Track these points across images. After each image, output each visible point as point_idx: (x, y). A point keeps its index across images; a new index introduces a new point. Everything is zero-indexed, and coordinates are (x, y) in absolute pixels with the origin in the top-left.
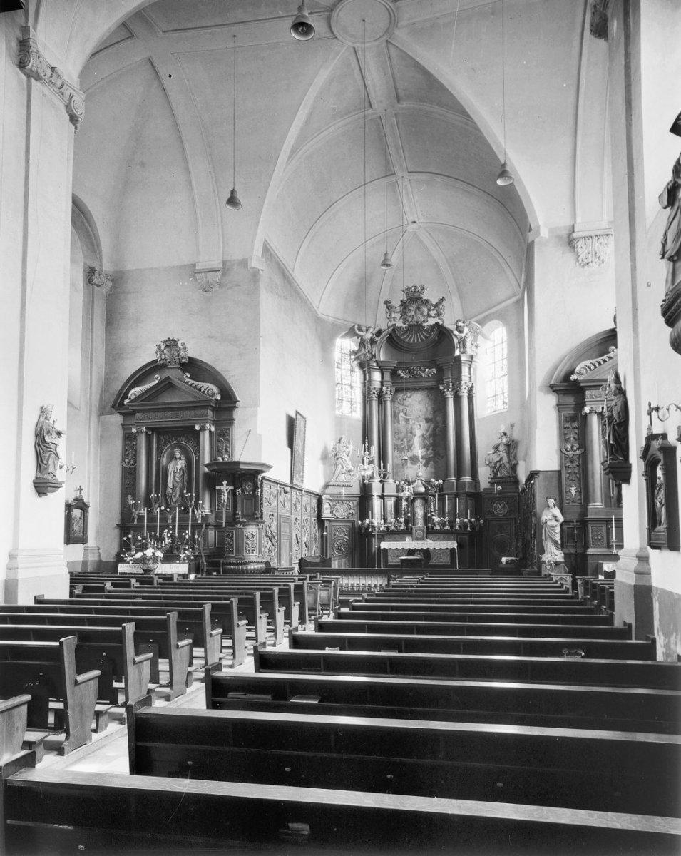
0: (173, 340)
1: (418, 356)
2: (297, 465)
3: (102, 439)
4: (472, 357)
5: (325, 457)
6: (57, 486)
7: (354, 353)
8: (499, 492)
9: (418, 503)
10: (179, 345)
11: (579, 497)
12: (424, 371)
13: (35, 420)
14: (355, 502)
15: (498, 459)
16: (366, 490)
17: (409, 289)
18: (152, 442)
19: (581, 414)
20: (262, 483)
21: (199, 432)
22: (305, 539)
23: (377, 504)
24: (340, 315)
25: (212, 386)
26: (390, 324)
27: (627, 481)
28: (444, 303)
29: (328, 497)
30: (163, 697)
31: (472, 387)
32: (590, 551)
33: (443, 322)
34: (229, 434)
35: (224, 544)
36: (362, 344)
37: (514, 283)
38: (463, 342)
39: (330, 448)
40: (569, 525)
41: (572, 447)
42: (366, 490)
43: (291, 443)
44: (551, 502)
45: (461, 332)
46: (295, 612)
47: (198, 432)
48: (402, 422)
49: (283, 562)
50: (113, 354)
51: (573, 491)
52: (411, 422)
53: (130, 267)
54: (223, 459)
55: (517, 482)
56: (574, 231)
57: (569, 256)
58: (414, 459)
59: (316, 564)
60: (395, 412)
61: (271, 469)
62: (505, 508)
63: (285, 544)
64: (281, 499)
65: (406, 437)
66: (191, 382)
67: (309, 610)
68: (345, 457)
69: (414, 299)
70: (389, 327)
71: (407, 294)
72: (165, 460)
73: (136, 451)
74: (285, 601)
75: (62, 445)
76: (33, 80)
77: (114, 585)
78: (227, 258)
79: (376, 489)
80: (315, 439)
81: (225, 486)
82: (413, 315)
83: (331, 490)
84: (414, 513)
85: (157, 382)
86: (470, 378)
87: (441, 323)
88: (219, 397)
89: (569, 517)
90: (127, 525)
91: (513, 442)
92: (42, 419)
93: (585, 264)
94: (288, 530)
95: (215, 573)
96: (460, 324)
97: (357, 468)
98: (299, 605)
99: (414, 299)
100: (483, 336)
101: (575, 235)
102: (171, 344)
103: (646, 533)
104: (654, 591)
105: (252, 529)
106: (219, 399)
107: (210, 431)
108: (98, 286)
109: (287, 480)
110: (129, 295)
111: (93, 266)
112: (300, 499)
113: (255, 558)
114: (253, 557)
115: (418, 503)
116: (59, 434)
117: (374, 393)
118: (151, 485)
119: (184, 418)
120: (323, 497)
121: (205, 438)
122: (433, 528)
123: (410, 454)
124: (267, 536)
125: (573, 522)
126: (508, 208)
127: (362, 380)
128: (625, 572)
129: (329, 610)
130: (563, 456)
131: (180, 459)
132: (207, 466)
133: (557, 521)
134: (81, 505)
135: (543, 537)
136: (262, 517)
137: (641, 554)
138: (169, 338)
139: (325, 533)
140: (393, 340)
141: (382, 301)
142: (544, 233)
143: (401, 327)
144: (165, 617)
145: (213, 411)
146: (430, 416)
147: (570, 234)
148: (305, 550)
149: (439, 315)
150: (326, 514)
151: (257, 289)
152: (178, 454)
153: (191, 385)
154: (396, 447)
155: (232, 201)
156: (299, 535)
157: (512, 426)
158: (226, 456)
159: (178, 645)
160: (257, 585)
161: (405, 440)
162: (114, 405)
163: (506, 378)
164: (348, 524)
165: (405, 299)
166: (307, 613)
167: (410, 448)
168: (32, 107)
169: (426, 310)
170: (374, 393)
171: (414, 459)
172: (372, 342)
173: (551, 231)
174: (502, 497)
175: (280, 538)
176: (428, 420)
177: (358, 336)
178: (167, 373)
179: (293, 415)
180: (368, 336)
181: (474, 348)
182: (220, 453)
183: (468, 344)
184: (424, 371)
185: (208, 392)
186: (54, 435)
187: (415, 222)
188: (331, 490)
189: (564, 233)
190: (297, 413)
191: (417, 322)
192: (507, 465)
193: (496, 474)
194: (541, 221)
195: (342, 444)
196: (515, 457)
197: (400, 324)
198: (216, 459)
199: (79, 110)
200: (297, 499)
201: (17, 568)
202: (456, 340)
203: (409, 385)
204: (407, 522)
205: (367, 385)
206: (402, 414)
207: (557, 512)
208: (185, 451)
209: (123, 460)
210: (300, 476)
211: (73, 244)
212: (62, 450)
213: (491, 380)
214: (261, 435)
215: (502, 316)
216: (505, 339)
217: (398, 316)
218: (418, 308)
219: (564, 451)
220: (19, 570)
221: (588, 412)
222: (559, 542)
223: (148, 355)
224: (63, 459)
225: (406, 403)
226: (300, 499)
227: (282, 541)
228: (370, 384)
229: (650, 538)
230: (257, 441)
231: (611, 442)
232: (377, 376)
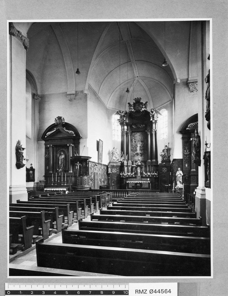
0: (60, 117)
1: (138, 121)
2: (100, 156)
3: (39, 148)
4: (156, 121)
5: (109, 154)
6: (23, 165)
7: (118, 120)
8: (164, 165)
9: (139, 168)
10: (62, 118)
11: (188, 168)
12: (141, 126)
13: (16, 145)
14: (119, 168)
15: (164, 154)
16: (122, 164)
17: (136, 99)
20: (88, 163)
21: (68, 146)
22: (103, 180)
23: (126, 168)
24: (114, 107)
25: (72, 132)
26: (130, 110)
27: (200, 166)
28: (147, 103)
29: (110, 166)
30: (55, 232)
31: (156, 131)
32: (191, 185)
33: (147, 109)
36: (121, 117)
37: (170, 97)
38: (153, 116)
39: (111, 150)
40: (185, 176)
41: (187, 151)
42: (122, 164)
43: (98, 149)
44: (179, 169)
45: (153, 113)
46: (97, 204)
48: (134, 142)
49: (95, 187)
50: (41, 121)
51: (187, 166)
52: (137, 142)
53: (46, 93)
54: (76, 155)
55: (170, 161)
56: (188, 80)
57: (186, 89)
58: (137, 154)
59: (105, 188)
60: (131, 139)
61: (91, 158)
62: (166, 170)
63: (96, 181)
64: (95, 167)
65: (135, 147)
66: (66, 130)
67: (102, 203)
68: (115, 153)
69: (138, 102)
70: (129, 111)
71: (135, 101)
72: (58, 155)
73: (49, 152)
74: (94, 201)
75: (24, 153)
76: (12, 36)
77: (42, 196)
78: (77, 90)
79: (125, 163)
80: (106, 148)
83: (111, 164)
84: (137, 171)
85: (55, 130)
86: (155, 128)
87: (146, 110)
88: (75, 135)
89: (185, 174)
90: (47, 175)
91: (169, 148)
92: (18, 145)
93: (192, 91)
94: (97, 177)
95: (74, 191)
96: (152, 110)
97: (118, 158)
98: (99, 202)
99: (138, 102)
100: (160, 114)
101: (188, 82)
102: (60, 118)
103: (204, 182)
104: (206, 200)
105: (85, 177)
107: (72, 146)
108: (36, 99)
109: (97, 161)
110: (46, 102)
111: (34, 93)
112: (101, 167)
113: (87, 187)
114: (87, 186)
115: (139, 168)
116: (23, 149)
117: (125, 133)
119: (64, 142)
120: (109, 166)
121: (71, 149)
122: (143, 176)
123: (136, 152)
124: (90, 179)
125: (186, 175)
126: (168, 74)
127: (121, 129)
128: (198, 194)
129: (108, 203)
130: (184, 154)
131: (63, 155)
132: (71, 157)
133: (181, 175)
134: (32, 169)
135: (177, 180)
136: (88, 174)
137: (203, 189)
138: (59, 116)
139: (109, 178)
140: (130, 115)
141: (127, 103)
142: (179, 81)
143: (133, 111)
144: (55, 208)
145: (73, 140)
146: (142, 140)
147: (187, 81)
148: (103, 183)
149: (146, 107)
150: (110, 171)
151: (86, 100)
152: (62, 153)
153: (66, 131)
154: (132, 150)
155: (78, 72)
156: (101, 178)
157: (169, 143)
158: (77, 154)
159: (59, 217)
160: (86, 196)
161: (134, 148)
162: (42, 138)
163: (167, 128)
164: (116, 175)
165: (135, 102)
166: (101, 204)
167: (136, 150)
168: (12, 44)
169: (141, 106)
170: (125, 133)
171: (137, 154)
172: (124, 116)
173: (181, 80)
174: (165, 166)
175: (96, 178)
176: (142, 142)
177: (120, 114)
178: (58, 128)
179: (99, 141)
180: (123, 114)
181: (157, 118)
182: (75, 153)
183: (155, 117)
184: (141, 126)
186: (22, 150)
187: (138, 77)
188: (111, 164)
189: (185, 81)
190: (100, 140)
191: (138, 110)
192: (167, 156)
193: (163, 159)
194: (178, 77)
195: (114, 149)
196: (169, 154)
197: (133, 110)
198: (74, 155)
199: (28, 44)
200: (100, 167)
201: (11, 191)
202: (151, 116)
203: (136, 130)
204: (135, 174)
205: (123, 130)
206: (133, 140)
207: (181, 172)
209: (45, 155)
210: (101, 160)
211: (27, 86)
212: (24, 155)
213: (162, 128)
214: (88, 148)
215: (166, 107)
216: (167, 115)
217: (132, 108)
218: (139, 105)
219: (184, 153)
220: (12, 192)
221: (192, 140)
222: (182, 182)
223: (52, 122)
224: (25, 157)
225: (135, 136)
226: (101, 167)
227: (95, 181)
228: (123, 130)
229: (205, 184)
230: (87, 149)
231: (195, 153)
232: (126, 127)
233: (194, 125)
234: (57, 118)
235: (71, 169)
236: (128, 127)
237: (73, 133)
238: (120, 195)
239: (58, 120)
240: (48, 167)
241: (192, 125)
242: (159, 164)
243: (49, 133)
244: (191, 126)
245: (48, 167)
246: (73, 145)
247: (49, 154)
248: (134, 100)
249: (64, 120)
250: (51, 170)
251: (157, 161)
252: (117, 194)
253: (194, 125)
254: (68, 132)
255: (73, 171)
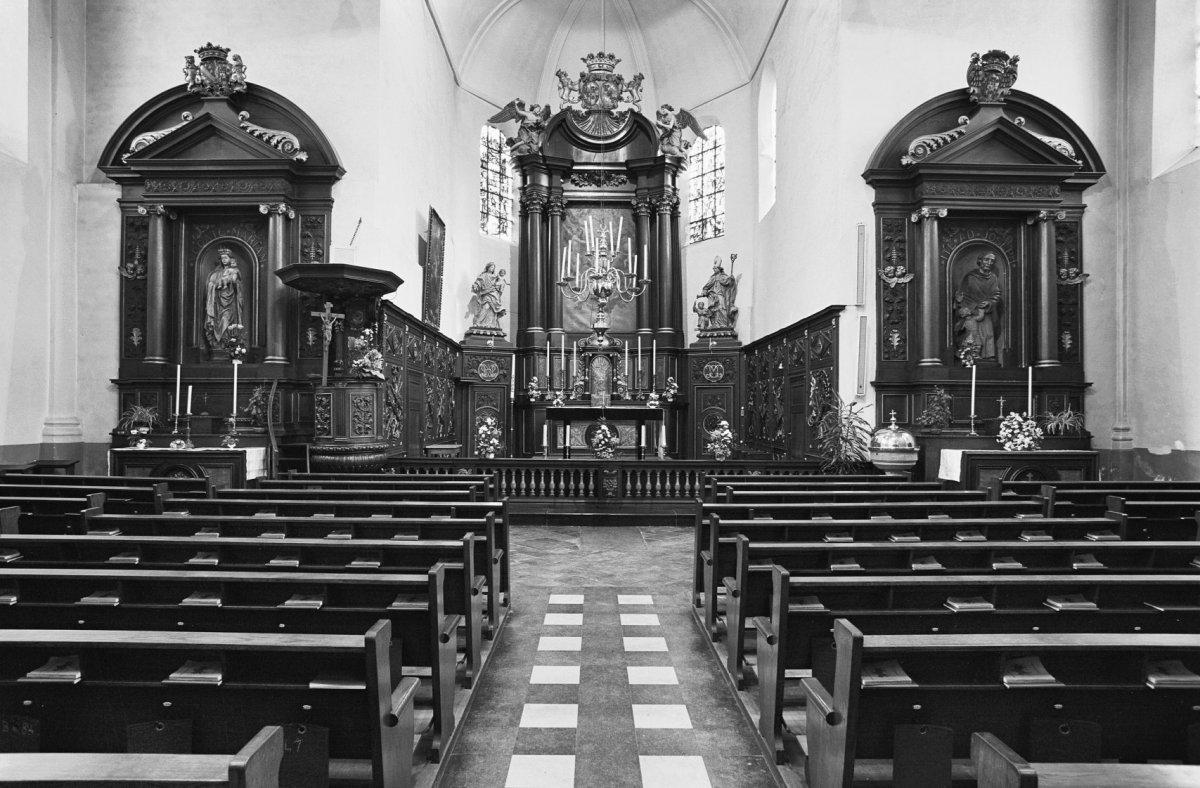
0: (217, 48)
3: (81, 223)
10: (230, 59)
18: (178, 236)
19: (910, 220)
31: (678, 203)
34: (321, 224)
35: (313, 417)
47: (266, 218)
66: (252, 127)
73: (146, 249)
81: (328, 311)
82: (597, 96)
87: (636, 110)
88: (303, 157)
102: (213, 55)
106: (304, 159)
118: (177, 297)
119: (235, 193)
121: (277, 227)
131: (229, 265)
132: (281, 274)
138: (209, 44)
144: (85, 499)
152: (226, 259)
162: (102, 164)
185: (283, 146)
197: (578, 107)
208: (238, 251)
209: (123, 266)
223: (175, 76)
233: (936, 142)
234: (196, 56)
235: (280, 348)
236: (554, 176)
237: (297, 145)
238: (644, 489)
239: (202, 67)
240: (136, 333)
241: (929, 145)
242: (687, 347)
243: (148, 138)
244: (925, 150)
245: (136, 333)
246: (292, 215)
247: (144, 258)
248: (584, 60)
249: (240, 66)
250: (159, 351)
251: (679, 334)
252: (538, 482)
253: (939, 145)
254: (265, 138)
255: (288, 354)
